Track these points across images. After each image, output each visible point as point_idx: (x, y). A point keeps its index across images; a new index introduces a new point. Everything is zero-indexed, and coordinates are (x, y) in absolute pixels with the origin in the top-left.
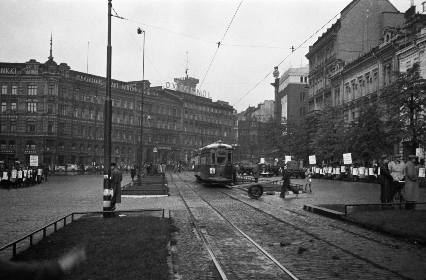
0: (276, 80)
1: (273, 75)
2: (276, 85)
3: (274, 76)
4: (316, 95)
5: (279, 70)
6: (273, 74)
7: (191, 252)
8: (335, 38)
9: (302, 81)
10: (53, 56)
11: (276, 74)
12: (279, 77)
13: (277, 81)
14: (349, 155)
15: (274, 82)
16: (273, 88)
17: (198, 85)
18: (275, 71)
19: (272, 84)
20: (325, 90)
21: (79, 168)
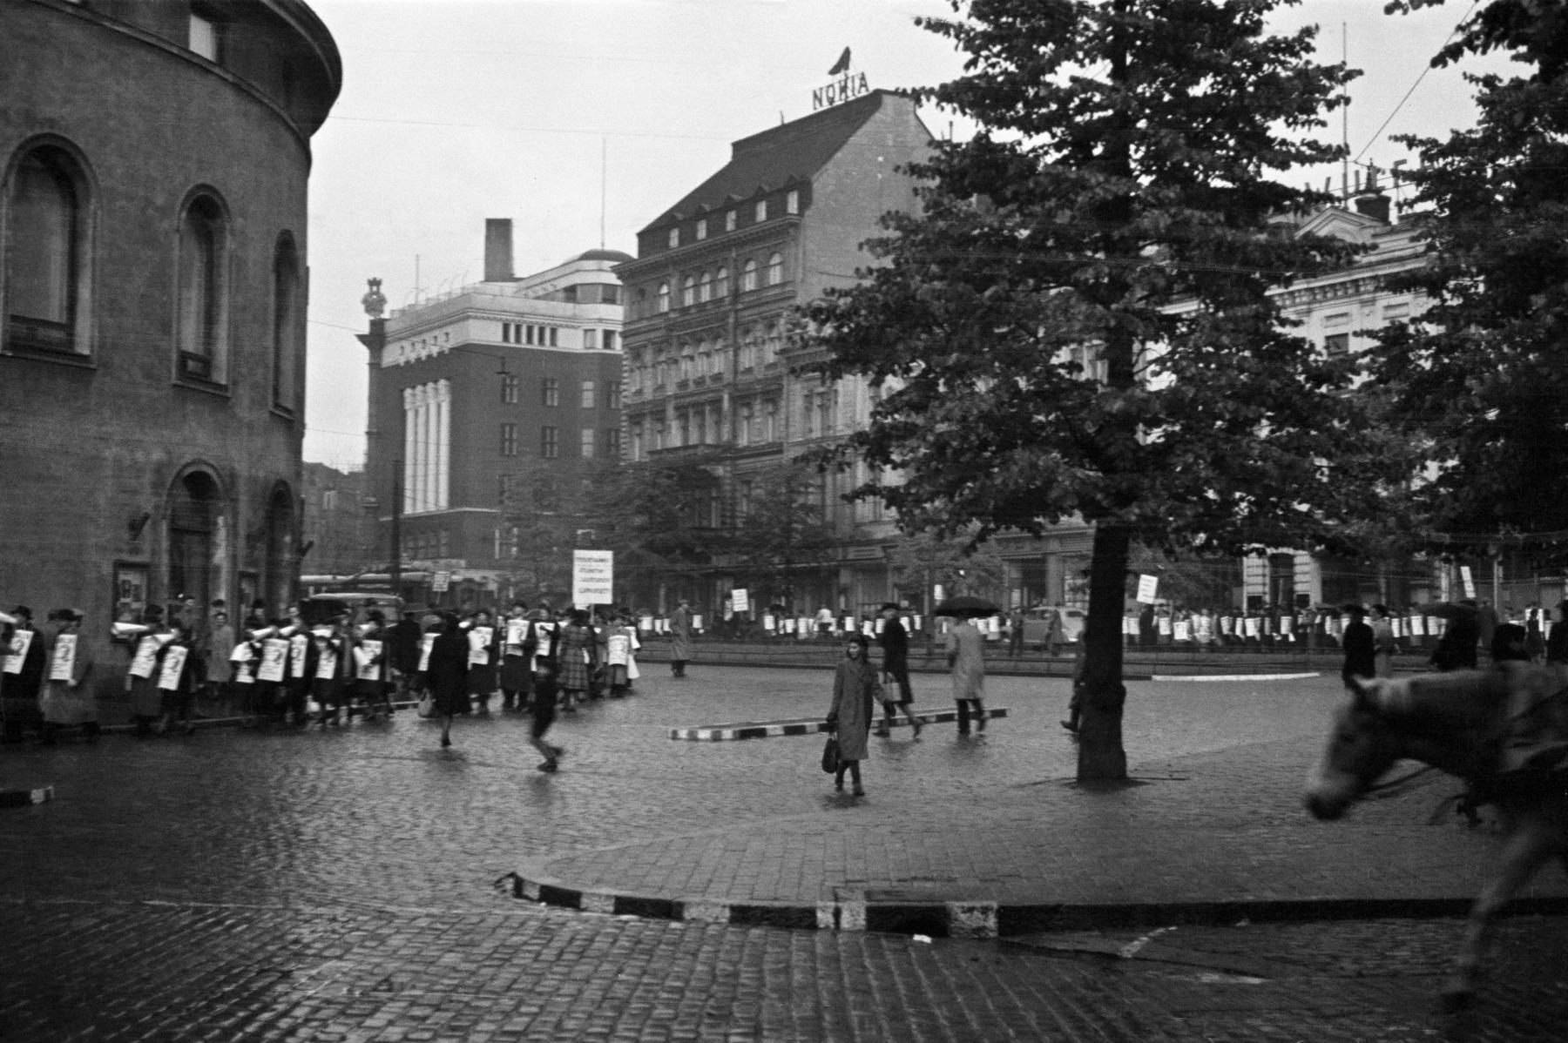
0: (373, 323)
1: (362, 307)
2: (376, 339)
3: (368, 310)
4: (676, 397)
5: (383, 290)
6: (365, 301)
7: (590, 968)
8: (791, 231)
9: (506, 337)
10: (1481, 75)
11: (374, 303)
12: (386, 315)
13: (378, 325)
14: (1154, 580)
15: (365, 329)
16: (364, 353)
17: (366, 330)
18: (372, 293)
19: (362, 338)
20: (733, 385)
21: (1530, 865)
